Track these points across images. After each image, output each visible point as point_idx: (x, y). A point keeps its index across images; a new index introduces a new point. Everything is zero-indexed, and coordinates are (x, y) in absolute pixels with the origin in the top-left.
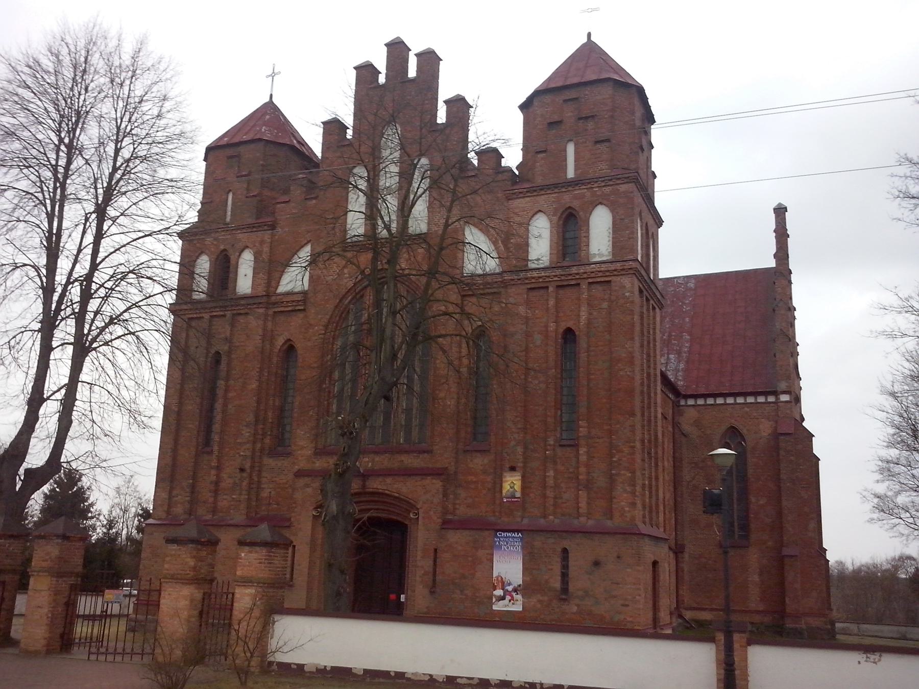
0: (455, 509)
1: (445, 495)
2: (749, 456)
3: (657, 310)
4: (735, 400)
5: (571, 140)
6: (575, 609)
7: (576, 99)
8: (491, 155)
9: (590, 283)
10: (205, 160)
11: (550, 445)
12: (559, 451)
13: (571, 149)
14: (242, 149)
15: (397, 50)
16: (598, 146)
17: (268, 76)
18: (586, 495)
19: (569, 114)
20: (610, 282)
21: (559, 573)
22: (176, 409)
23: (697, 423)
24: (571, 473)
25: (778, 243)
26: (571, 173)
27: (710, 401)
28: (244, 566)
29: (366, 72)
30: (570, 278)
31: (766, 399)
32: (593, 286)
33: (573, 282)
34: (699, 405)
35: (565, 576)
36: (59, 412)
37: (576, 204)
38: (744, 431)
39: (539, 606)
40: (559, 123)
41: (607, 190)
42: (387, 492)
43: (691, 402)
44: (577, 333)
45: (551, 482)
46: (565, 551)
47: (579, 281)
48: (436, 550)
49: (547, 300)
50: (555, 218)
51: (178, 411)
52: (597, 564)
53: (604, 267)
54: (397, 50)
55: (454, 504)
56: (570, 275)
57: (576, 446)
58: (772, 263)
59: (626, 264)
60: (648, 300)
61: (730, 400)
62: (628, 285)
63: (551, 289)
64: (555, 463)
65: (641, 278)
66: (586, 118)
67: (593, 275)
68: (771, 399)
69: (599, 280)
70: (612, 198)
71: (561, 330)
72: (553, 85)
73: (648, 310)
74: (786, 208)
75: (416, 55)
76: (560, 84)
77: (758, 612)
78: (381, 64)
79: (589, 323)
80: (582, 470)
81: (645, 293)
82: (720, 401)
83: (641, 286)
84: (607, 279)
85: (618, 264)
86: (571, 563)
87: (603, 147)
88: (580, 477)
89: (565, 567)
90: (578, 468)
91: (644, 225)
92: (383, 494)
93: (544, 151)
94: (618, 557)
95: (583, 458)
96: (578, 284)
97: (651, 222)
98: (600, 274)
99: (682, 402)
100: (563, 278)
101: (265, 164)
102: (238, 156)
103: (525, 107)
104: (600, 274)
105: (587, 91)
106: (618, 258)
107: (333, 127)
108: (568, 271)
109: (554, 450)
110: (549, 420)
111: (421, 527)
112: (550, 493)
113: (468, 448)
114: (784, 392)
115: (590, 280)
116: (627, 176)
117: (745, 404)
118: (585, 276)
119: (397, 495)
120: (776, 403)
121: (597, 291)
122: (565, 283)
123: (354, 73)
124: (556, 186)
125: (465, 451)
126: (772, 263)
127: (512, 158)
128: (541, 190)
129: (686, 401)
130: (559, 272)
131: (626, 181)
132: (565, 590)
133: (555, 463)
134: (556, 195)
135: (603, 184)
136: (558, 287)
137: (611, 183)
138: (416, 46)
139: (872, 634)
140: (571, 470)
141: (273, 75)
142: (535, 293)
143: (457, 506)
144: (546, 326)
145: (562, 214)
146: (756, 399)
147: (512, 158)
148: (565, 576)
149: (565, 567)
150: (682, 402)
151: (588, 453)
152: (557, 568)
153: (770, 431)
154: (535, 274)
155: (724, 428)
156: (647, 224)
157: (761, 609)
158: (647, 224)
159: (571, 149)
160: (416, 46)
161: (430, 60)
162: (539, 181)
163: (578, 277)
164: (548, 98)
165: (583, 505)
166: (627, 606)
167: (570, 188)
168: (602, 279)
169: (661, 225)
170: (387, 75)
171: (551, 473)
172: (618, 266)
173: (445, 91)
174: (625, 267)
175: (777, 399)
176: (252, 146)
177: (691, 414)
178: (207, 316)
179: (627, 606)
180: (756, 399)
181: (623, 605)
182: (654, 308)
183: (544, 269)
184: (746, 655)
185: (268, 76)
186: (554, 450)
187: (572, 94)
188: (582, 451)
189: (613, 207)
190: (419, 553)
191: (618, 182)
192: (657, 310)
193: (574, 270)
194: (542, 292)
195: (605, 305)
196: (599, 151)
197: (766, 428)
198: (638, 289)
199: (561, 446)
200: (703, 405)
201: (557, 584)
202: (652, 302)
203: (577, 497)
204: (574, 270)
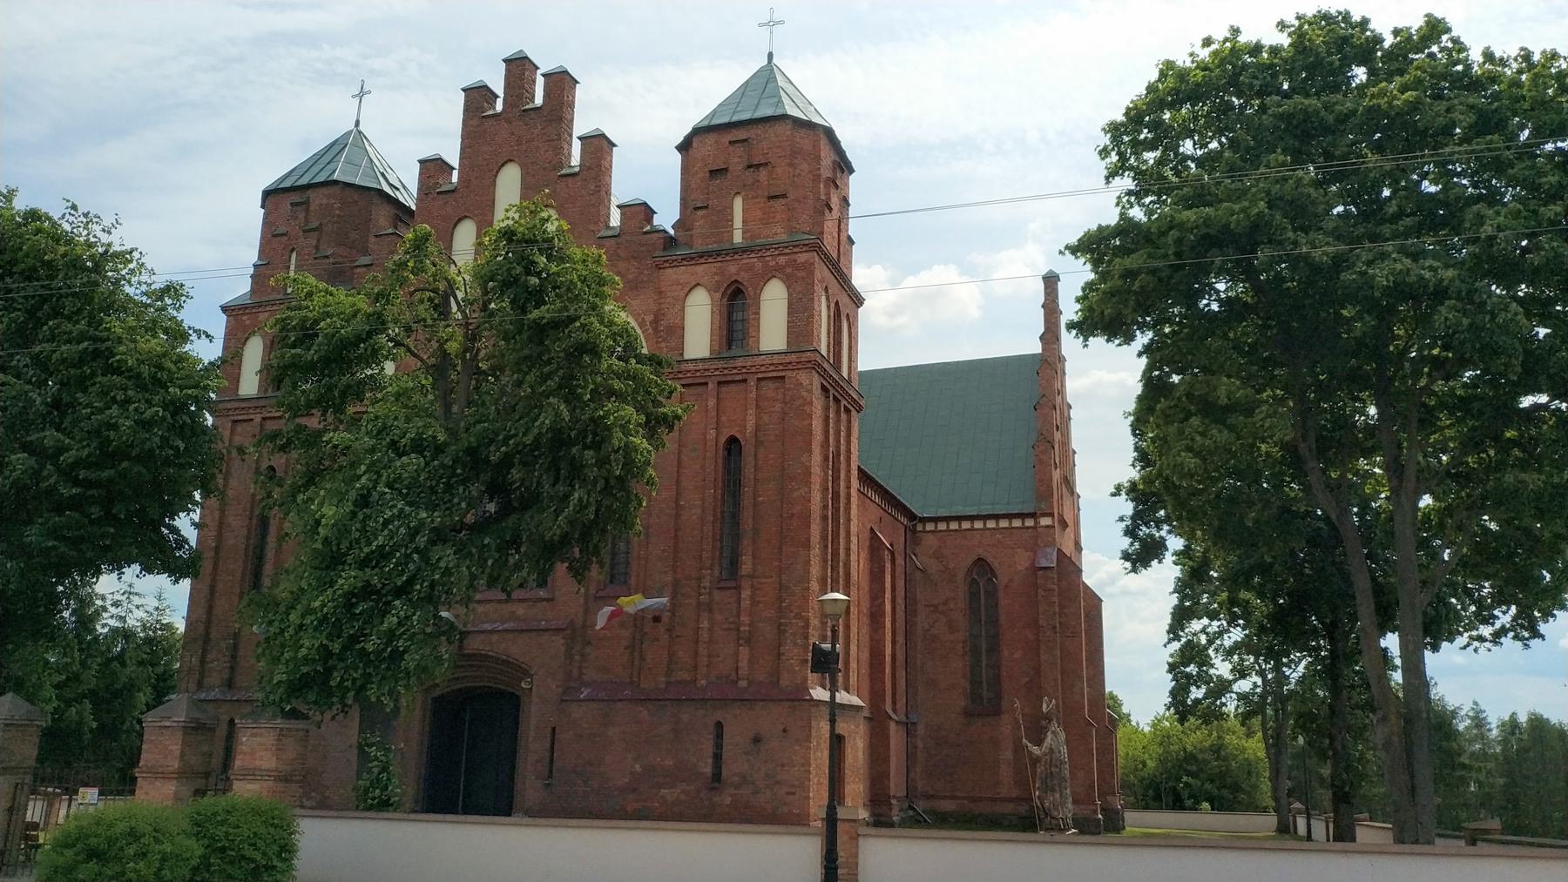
0: (581, 674)
1: (569, 655)
2: (1001, 594)
3: (854, 413)
4: (985, 524)
5: (738, 193)
6: (728, 800)
7: (746, 140)
8: (641, 212)
9: (759, 379)
10: (263, 207)
11: (705, 588)
12: (717, 595)
13: (738, 204)
14: (311, 194)
15: (518, 67)
16: (772, 202)
17: (354, 97)
18: (747, 651)
19: (736, 160)
20: (783, 378)
21: (711, 754)
22: (214, 544)
23: (938, 555)
24: (731, 623)
25: (1047, 321)
26: (738, 238)
27: (954, 526)
28: (245, 754)
29: (477, 96)
30: (735, 371)
31: (1023, 523)
32: (763, 383)
33: (737, 378)
34: (940, 531)
35: (717, 757)
36: (849, 382)
37: (743, 277)
38: (995, 564)
39: (683, 797)
40: (723, 171)
41: (782, 260)
42: (490, 653)
43: (930, 527)
44: (743, 443)
45: (705, 636)
46: (719, 725)
47: (745, 376)
48: (554, 729)
49: (707, 400)
50: (718, 295)
51: (217, 547)
52: (757, 740)
53: (776, 360)
54: (518, 67)
55: (580, 668)
56: (735, 368)
57: (738, 588)
58: (1037, 348)
59: (804, 355)
60: (837, 401)
61: (978, 525)
62: (805, 382)
63: (711, 386)
64: (710, 611)
65: (823, 374)
66: (758, 166)
67: (763, 369)
68: (1029, 523)
69: (770, 375)
70: (788, 270)
71: (723, 439)
72: (717, 121)
73: (838, 412)
74: (1058, 276)
75: (543, 75)
76: (725, 120)
77: (1010, 800)
78: (498, 87)
79: (758, 428)
80: (745, 619)
81: (832, 391)
82: (966, 525)
83: (825, 383)
84: (780, 374)
85: (793, 356)
86: (725, 741)
87: (778, 204)
88: (742, 629)
89: (719, 745)
90: (738, 615)
91: (833, 305)
92: (486, 656)
93: (706, 207)
94: (785, 731)
95: (746, 603)
96: (745, 381)
97: (844, 300)
98: (772, 368)
99: (919, 527)
100: (726, 372)
101: (342, 214)
102: (306, 203)
103: (685, 147)
104: (772, 368)
105: (758, 131)
106: (794, 349)
107: (432, 168)
108: (731, 364)
109: (710, 594)
110: (705, 555)
111: (535, 699)
112: (702, 650)
113: (601, 594)
114: (1044, 515)
115: (760, 376)
116: (807, 242)
117: (948, 530)
118: (753, 370)
119: (505, 658)
120: (1034, 528)
121: (769, 389)
122: (729, 378)
123: (460, 98)
124: (718, 253)
125: (597, 598)
126: (1037, 348)
127: (667, 216)
128: (701, 257)
129: (924, 526)
130: (720, 364)
131: (805, 249)
132: (717, 776)
133: (710, 611)
134: (720, 264)
135: (777, 252)
136: (719, 383)
137: (787, 251)
138: (545, 64)
139: (1542, 850)
140: (731, 620)
141: (361, 94)
142: (692, 390)
143: (584, 671)
144: (705, 434)
145: (726, 289)
146: (997, 523)
147: (667, 216)
148: (717, 757)
149: (719, 745)
150: (919, 527)
151: (752, 597)
152: (708, 747)
153: (1027, 564)
154: (691, 366)
155: (970, 561)
156: (837, 303)
157: (1014, 795)
158: (837, 303)
159: (738, 204)
160: (545, 64)
161: (561, 83)
162: (699, 246)
163: (744, 371)
164: (711, 139)
165: (744, 664)
166: (794, 793)
167: (736, 257)
168: (775, 374)
169: (862, 304)
170: (505, 100)
171: (705, 624)
172: (793, 358)
173: (582, 124)
174: (803, 360)
175: (1036, 522)
176: (324, 191)
177: (930, 542)
178: (258, 418)
179: (794, 793)
180: (997, 523)
181: (788, 793)
182: (847, 411)
183: (703, 360)
184: (857, 846)
185: (354, 97)
186: (710, 594)
187: (741, 134)
188: (746, 594)
189: (789, 281)
190: (532, 733)
191: (795, 250)
192: (854, 413)
193: (739, 362)
194: (701, 389)
195: (778, 407)
196: (773, 209)
197: (1022, 560)
198: (819, 387)
199: (718, 589)
200: (946, 531)
201: (708, 770)
202: (844, 402)
203: (737, 654)
204: (739, 362)
